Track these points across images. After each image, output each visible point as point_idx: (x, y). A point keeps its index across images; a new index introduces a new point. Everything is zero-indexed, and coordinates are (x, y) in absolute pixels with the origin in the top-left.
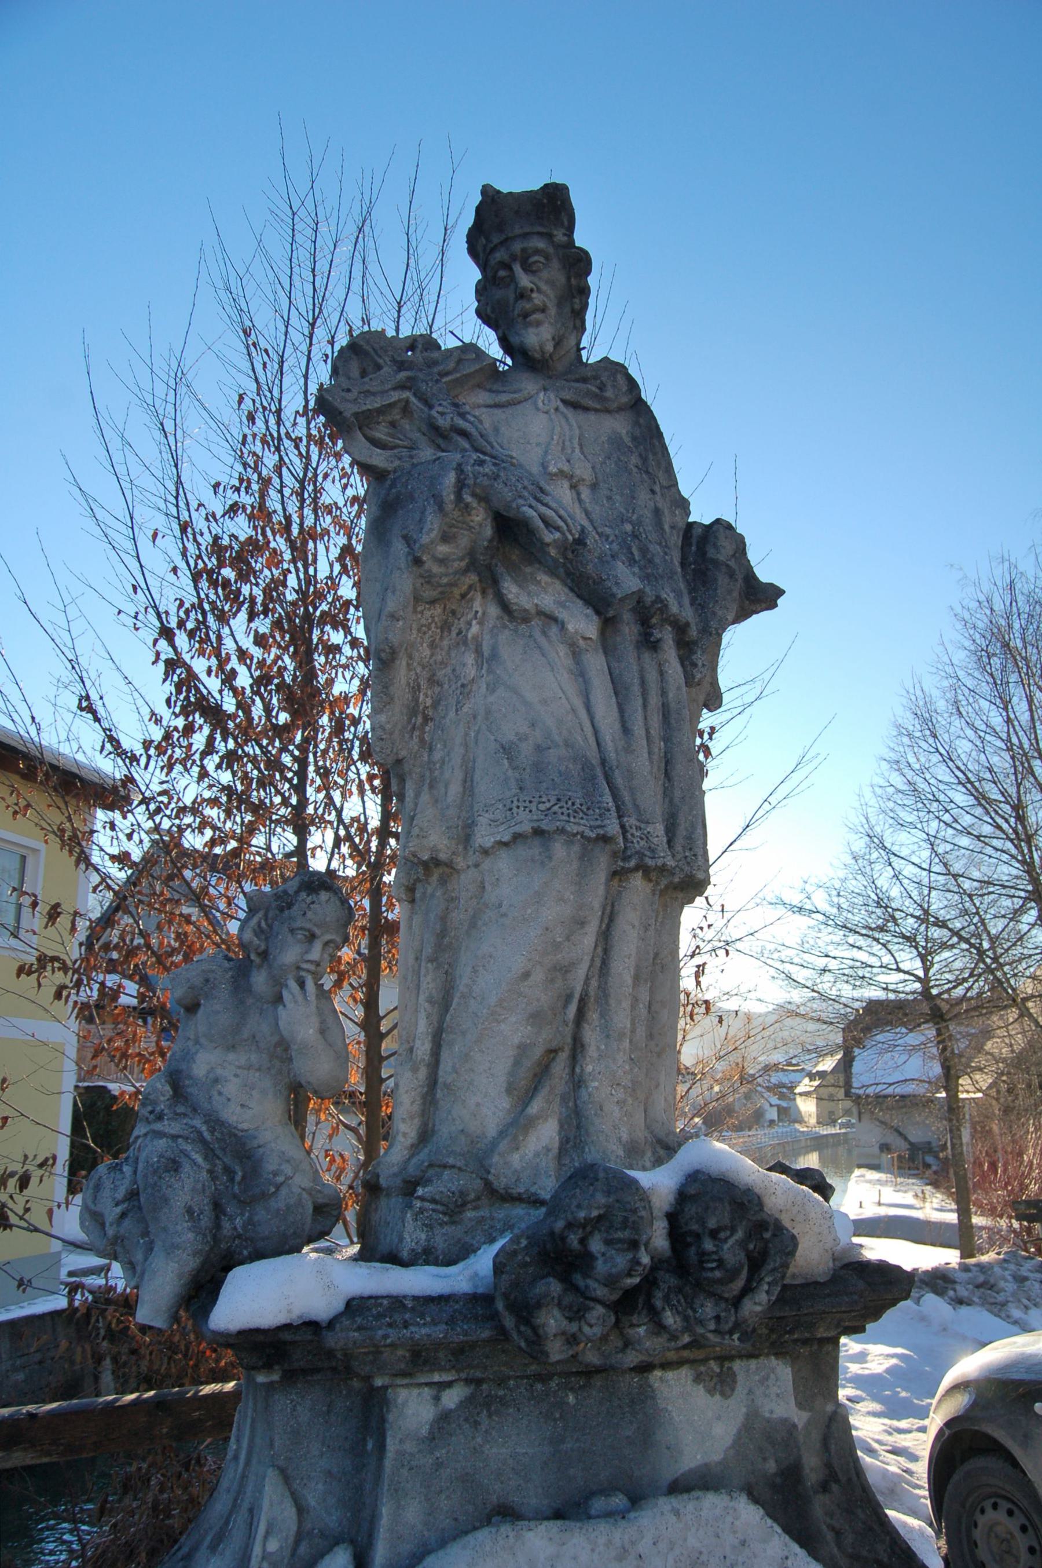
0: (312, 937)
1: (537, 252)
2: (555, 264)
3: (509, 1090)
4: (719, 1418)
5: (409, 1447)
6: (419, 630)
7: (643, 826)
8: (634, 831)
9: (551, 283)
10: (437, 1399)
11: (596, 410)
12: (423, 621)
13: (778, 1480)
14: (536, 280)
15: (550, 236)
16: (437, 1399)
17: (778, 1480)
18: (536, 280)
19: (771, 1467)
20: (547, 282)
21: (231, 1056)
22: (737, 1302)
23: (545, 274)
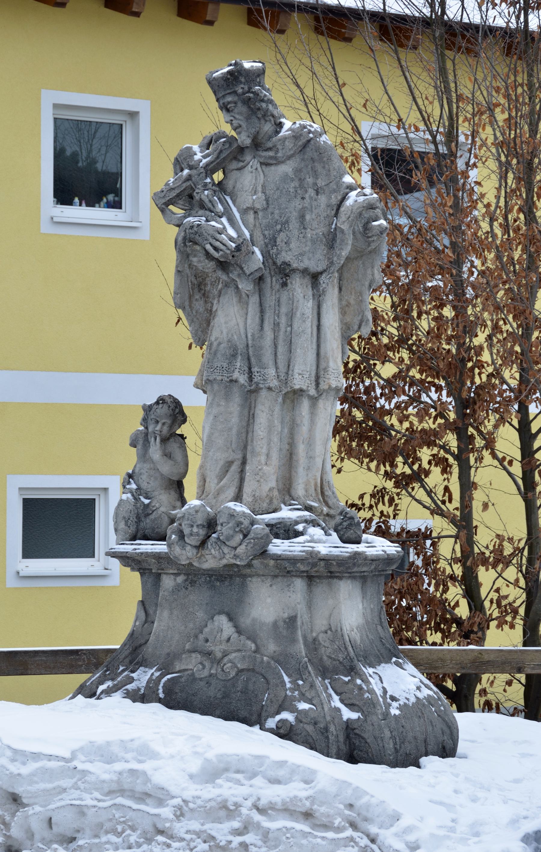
0: (157, 422)
1: (229, 103)
2: (240, 104)
3: (217, 477)
4: (269, 597)
5: (166, 593)
6: (211, 284)
7: (262, 370)
8: (256, 374)
9: (240, 113)
10: (175, 580)
11: (276, 164)
12: (213, 280)
13: (287, 620)
14: (233, 114)
15: (235, 92)
16: (175, 580)
17: (287, 620)
18: (233, 114)
19: (286, 615)
20: (238, 114)
21: (145, 465)
22: (235, 548)
23: (236, 110)
